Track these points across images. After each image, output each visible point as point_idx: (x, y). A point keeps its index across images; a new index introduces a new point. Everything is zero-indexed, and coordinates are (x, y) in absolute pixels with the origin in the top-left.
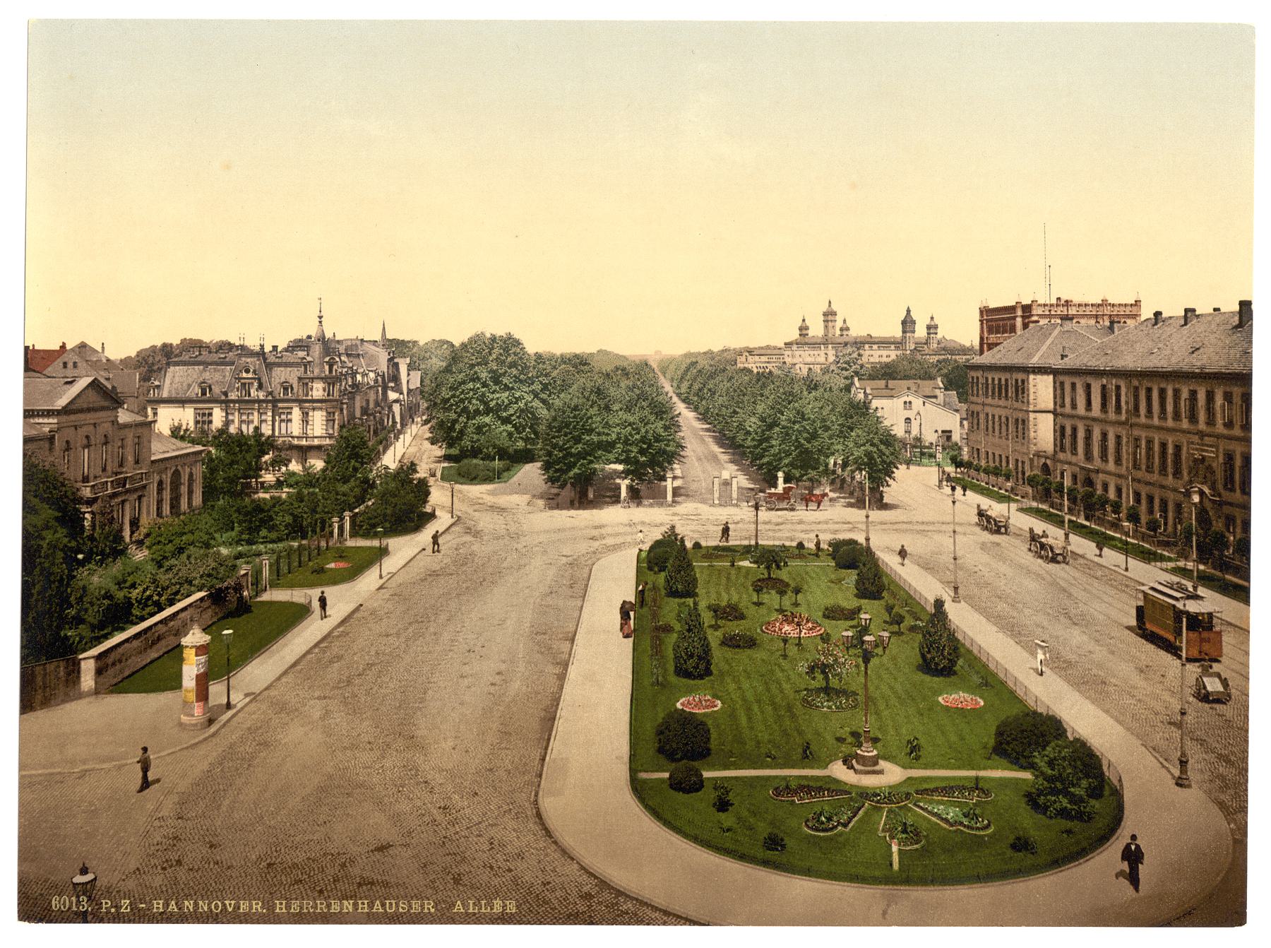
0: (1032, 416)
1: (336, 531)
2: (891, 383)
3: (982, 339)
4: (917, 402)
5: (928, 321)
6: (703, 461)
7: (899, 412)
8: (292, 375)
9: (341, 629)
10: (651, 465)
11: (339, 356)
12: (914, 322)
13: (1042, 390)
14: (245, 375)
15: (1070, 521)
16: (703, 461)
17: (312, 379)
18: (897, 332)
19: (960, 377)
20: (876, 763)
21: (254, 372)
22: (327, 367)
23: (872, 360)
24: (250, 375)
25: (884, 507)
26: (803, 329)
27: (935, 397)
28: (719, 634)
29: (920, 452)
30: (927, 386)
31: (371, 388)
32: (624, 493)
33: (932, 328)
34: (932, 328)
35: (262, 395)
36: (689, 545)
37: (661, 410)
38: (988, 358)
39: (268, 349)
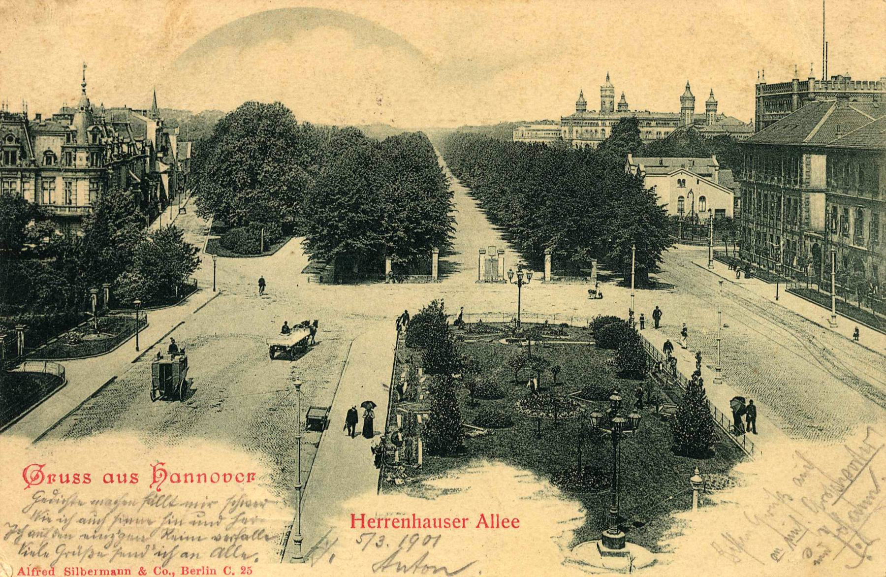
0: (804, 196)
1: (94, 302)
2: (667, 161)
3: (757, 116)
4: (691, 181)
5: (707, 98)
6: (473, 230)
7: (671, 188)
8: (55, 145)
9: (93, 400)
10: (418, 247)
11: (105, 125)
12: (693, 99)
13: (816, 167)
14: (7, 144)
15: (837, 301)
16: (473, 230)
17: (76, 149)
18: (675, 108)
19: (735, 153)
20: (623, 546)
21: (17, 140)
22: (90, 137)
23: (650, 136)
24: (13, 144)
25: (653, 286)
26: (582, 105)
27: (710, 175)
28: (475, 412)
29: (689, 229)
30: (702, 165)
31: (138, 158)
32: (388, 269)
33: (711, 105)
34: (711, 105)
35: (25, 164)
36: (451, 321)
37: (434, 186)
38: (765, 137)
39: (31, 117)
